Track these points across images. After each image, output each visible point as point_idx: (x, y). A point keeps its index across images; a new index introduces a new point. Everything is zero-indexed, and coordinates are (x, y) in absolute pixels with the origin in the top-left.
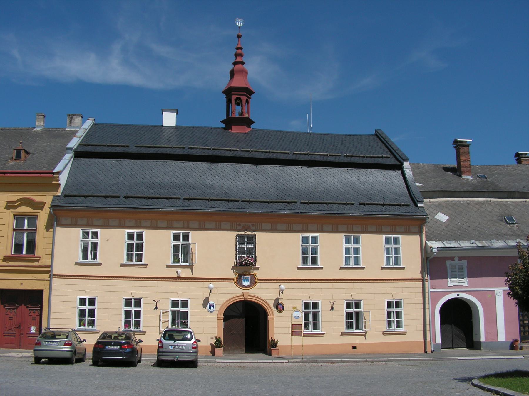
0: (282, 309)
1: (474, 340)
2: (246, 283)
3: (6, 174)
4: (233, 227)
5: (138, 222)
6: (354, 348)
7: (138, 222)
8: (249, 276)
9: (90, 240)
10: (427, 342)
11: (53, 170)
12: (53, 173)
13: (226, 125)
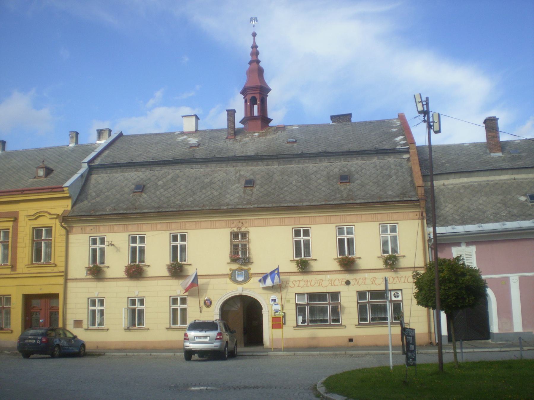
0: (209, 304)
1: (491, 331)
2: (240, 279)
3: (54, 189)
4: (281, 223)
5: (213, 224)
6: (351, 340)
7: (297, 221)
8: (243, 272)
9: (389, 235)
10: (501, 332)
11: (63, 184)
12: (63, 187)
13: (244, 125)
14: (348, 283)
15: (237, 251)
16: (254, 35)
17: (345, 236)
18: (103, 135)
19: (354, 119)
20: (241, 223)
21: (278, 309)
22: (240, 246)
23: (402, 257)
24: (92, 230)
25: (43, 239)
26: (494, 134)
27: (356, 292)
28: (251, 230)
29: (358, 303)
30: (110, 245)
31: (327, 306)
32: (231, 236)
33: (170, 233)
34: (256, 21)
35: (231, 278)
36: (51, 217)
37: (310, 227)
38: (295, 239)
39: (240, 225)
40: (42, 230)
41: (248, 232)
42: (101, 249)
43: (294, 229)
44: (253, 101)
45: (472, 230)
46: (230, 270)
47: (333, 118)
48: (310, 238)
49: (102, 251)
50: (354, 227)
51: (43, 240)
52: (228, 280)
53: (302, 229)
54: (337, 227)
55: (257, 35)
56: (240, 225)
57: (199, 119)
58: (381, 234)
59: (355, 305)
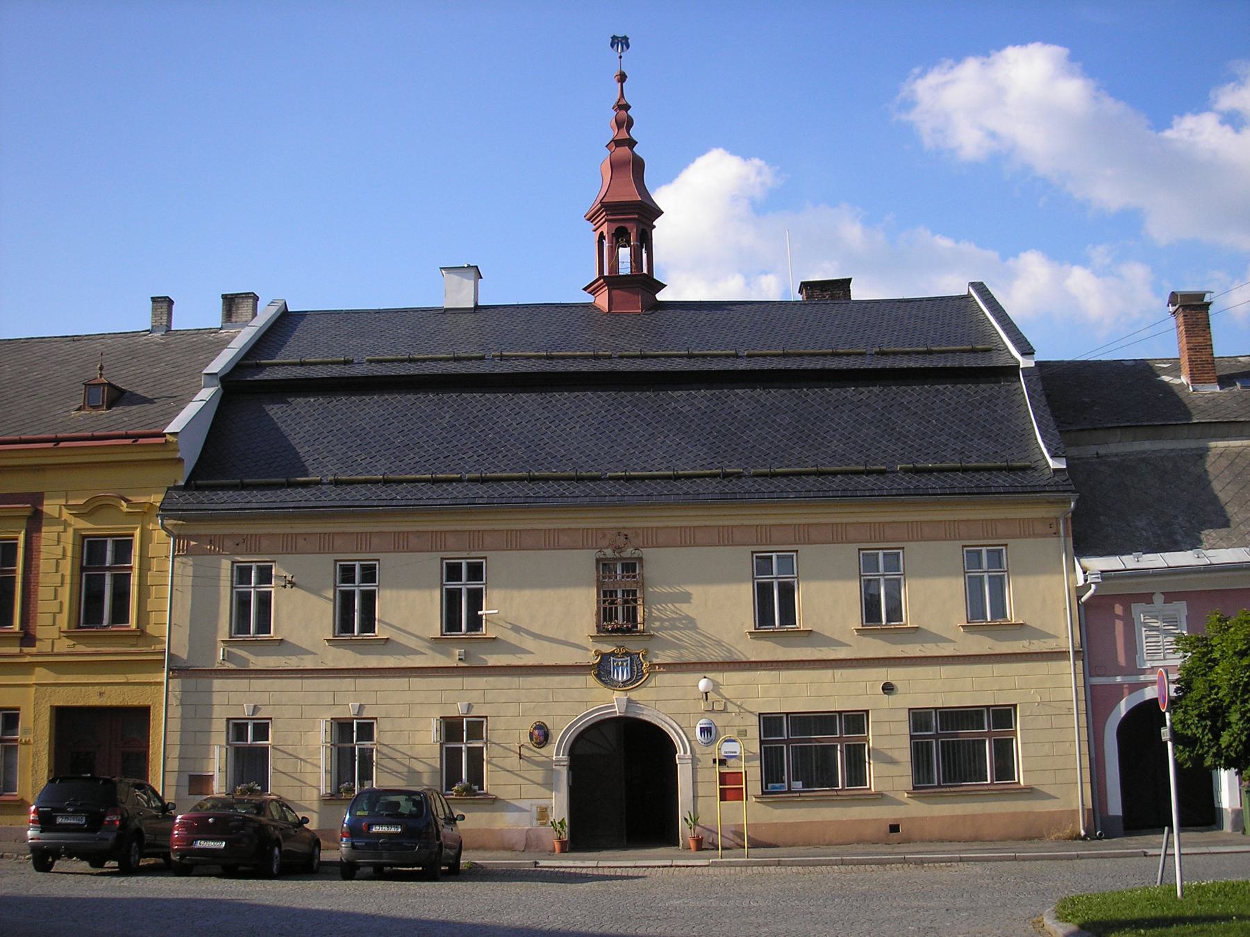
12: (164, 435)
14: (888, 688)
15: (614, 606)
16: (622, 78)
17: (463, 583)
18: (238, 309)
19: (857, 293)
20: (623, 538)
21: (734, 752)
22: (620, 595)
23: (914, 631)
24: (238, 545)
25: (107, 565)
26: (1201, 339)
27: (907, 710)
28: (647, 553)
29: (912, 737)
30: (289, 585)
31: (783, 747)
32: (597, 568)
33: (442, 559)
34: (624, 46)
35: (598, 676)
36: (71, 512)
37: (485, 558)
38: (447, 585)
39: (621, 541)
40: (106, 541)
41: (640, 559)
42: (364, 594)
43: (445, 561)
44: (620, 237)
45: (1181, 565)
46: (598, 653)
47: (806, 286)
48: (273, 587)
49: (265, 600)
50: (1006, 549)
51: (109, 569)
52: (591, 680)
53: (357, 564)
54: (755, 555)
55: (627, 79)
56: (621, 541)
57: (481, 278)
58: (234, 585)
59: (906, 742)
